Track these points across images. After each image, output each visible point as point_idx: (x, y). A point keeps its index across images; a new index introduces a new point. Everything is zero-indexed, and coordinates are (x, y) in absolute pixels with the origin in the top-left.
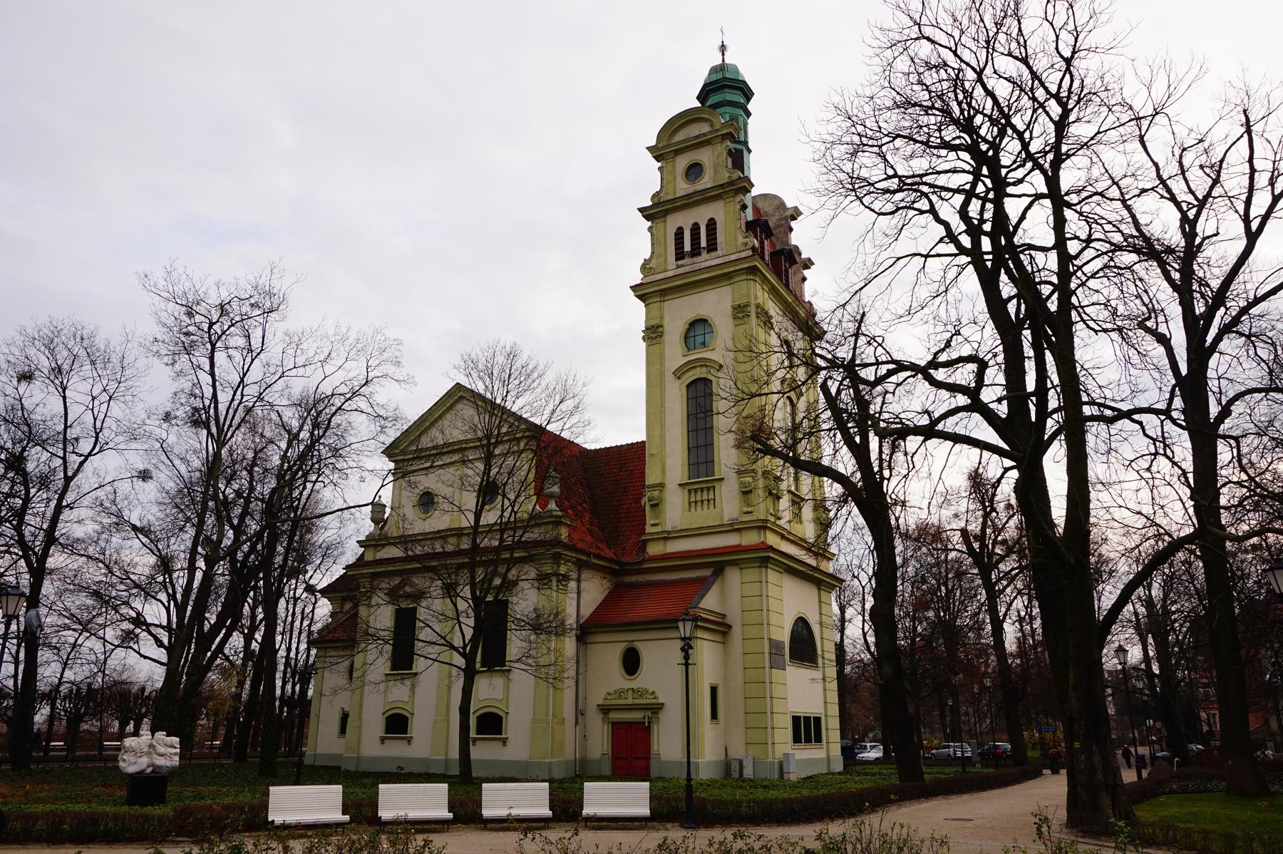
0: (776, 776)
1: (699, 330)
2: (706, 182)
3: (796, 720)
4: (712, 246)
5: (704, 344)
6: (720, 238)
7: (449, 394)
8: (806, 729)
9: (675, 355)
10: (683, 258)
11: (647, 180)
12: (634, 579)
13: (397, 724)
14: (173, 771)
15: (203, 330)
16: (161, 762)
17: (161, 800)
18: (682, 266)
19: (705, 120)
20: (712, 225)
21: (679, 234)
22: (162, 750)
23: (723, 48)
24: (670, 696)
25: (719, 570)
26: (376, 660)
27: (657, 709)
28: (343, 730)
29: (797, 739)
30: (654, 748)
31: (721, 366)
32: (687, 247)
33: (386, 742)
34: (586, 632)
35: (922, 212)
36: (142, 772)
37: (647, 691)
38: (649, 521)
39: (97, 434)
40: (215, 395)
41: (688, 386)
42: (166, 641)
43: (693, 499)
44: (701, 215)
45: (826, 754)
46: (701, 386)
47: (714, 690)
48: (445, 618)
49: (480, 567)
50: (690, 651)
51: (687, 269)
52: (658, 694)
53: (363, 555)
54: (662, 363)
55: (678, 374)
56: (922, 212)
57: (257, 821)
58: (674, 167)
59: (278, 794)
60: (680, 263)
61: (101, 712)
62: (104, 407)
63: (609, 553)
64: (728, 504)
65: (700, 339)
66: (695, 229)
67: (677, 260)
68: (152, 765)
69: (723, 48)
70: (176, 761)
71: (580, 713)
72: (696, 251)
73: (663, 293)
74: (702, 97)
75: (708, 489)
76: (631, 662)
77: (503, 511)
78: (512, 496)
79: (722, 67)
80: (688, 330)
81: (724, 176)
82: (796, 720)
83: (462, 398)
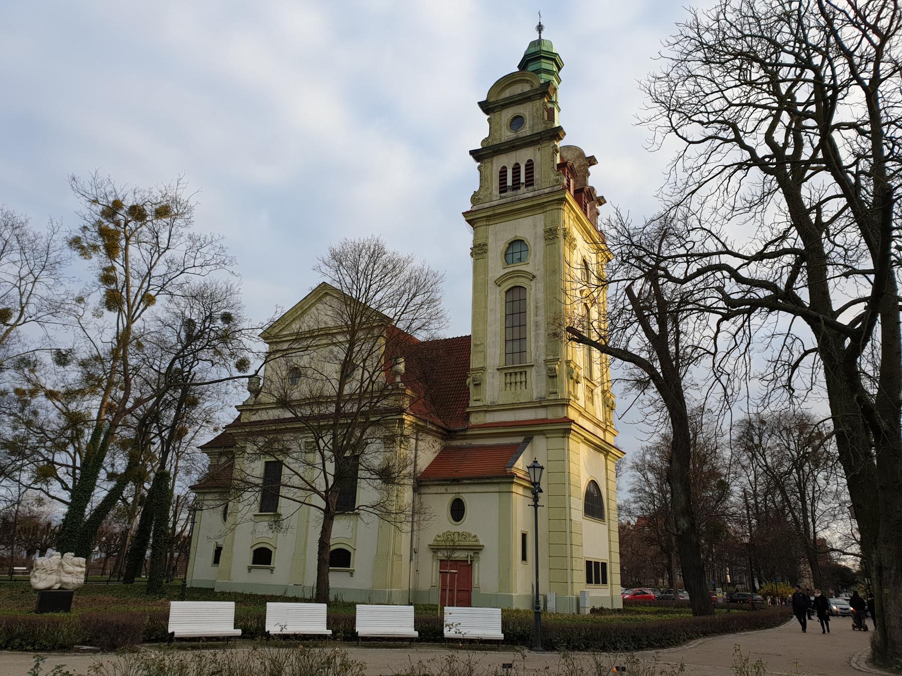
0: (575, 611)
1: (517, 248)
2: (526, 131)
3: (589, 563)
4: (530, 182)
5: (520, 260)
6: (536, 176)
7: (315, 292)
8: (596, 573)
9: (496, 267)
10: (506, 191)
11: (478, 129)
12: (464, 443)
13: (262, 557)
14: (79, 590)
15: (115, 226)
16: (68, 579)
17: (67, 609)
18: (505, 197)
19: (527, 81)
20: (530, 165)
21: (503, 172)
22: (71, 569)
23: (540, 28)
24: (487, 538)
25: (529, 438)
26: (250, 500)
27: (477, 549)
28: (216, 561)
29: (589, 581)
30: (475, 582)
31: (534, 277)
32: (509, 182)
33: (252, 570)
34: (421, 483)
35: (726, 141)
36: (50, 588)
37: (470, 535)
38: (473, 397)
39: (23, 308)
40: (127, 280)
41: (507, 292)
42: (70, 486)
43: (508, 381)
44: (523, 156)
45: (611, 594)
46: (516, 291)
47: (524, 536)
48: (309, 467)
49: (344, 427)
50: (540, 494)
51: (509, 199)
52: (479, 537)
53: (240, 416)
54: (486, 274)
55: (498, 283)
56: (726, 141)
57: (159, 635)
58: (501, 119)
59: (177, 608)
60: (503, 195)
61: (12, 543)
62: (29, 287)
63: (439, 422)
64: (536, 386)
65: (517, 256)
66: (516, 169)
67: (501, 192)
68: (61, 582)
69: (540, 28)
70: (81, 580)
71: (413, 551)
72: (516, 185)
73: (488, 218)
74: (523, 65)
75: (521, 373)
76: (458, 511)
77: (362, 383)
78: (371, 370)
79: (539, 42)
80: (508, 248)
81: (540, 128)
82: (589, 563)
83: (327, 294)
